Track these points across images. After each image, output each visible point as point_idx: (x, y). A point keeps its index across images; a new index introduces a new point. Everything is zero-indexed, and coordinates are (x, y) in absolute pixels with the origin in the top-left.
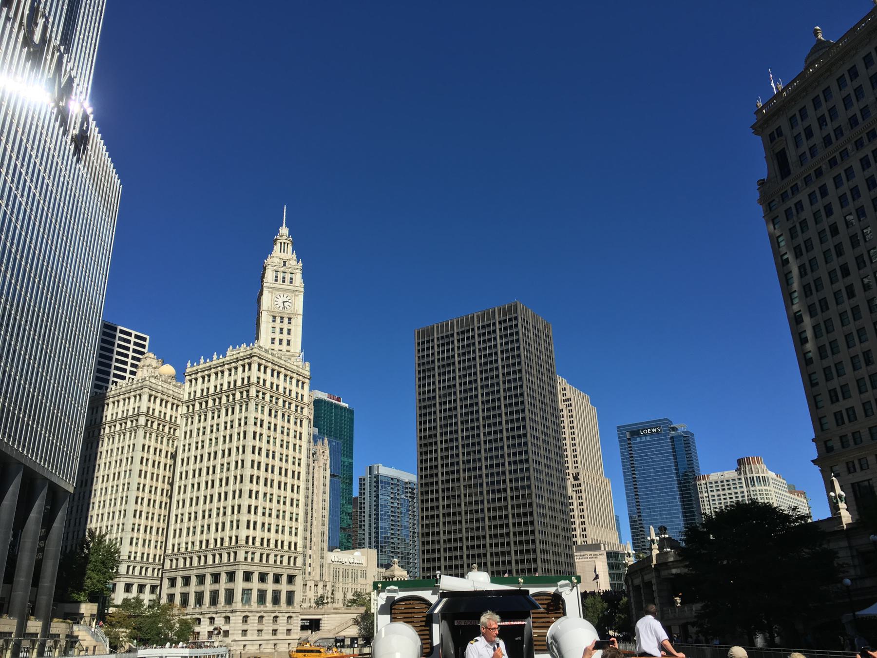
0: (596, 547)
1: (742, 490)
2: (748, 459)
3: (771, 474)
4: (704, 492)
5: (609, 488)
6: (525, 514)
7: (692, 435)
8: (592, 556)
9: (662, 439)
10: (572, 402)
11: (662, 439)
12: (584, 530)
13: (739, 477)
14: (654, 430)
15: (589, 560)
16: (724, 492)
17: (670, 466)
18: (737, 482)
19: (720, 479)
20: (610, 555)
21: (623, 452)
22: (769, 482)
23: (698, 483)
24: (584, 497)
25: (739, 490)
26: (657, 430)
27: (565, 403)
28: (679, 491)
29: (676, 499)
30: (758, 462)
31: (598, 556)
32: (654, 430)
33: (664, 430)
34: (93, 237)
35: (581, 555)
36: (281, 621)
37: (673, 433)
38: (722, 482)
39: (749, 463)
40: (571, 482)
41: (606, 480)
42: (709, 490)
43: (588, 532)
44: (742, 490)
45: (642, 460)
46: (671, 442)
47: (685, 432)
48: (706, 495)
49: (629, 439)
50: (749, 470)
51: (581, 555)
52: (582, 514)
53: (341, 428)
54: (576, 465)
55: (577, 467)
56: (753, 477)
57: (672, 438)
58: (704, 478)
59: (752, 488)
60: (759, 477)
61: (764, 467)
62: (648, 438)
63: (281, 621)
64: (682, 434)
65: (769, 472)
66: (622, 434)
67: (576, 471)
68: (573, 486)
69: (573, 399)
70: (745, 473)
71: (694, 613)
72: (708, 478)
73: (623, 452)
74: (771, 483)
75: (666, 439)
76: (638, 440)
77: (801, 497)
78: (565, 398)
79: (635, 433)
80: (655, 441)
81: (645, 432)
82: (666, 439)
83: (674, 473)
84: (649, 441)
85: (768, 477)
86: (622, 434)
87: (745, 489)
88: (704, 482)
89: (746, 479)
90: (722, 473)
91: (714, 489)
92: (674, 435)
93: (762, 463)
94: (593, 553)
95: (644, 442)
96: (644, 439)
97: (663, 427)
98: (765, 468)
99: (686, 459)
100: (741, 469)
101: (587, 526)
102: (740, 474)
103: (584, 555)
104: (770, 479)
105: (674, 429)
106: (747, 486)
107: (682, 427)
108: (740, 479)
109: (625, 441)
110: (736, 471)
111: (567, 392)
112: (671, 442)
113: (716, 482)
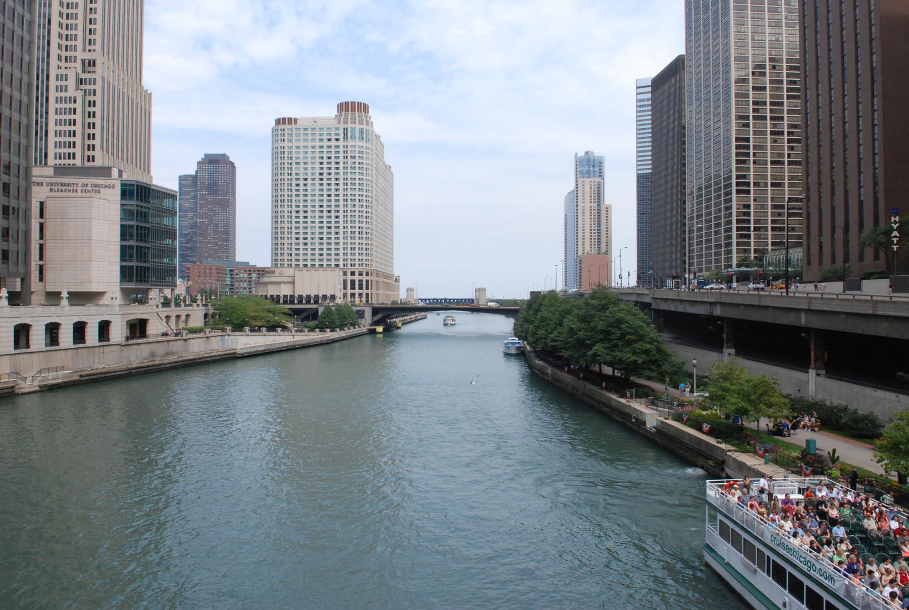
0: (105, 172)
1: (337, 143)
8: (89, 188)
13: (337, 126)
15: (79, 193)
31: (102, 190)
40: (77, 74)
50: (351, 119)
51: (62, 184)
68: (81, 81)
89: (345, 130)
103: (69, 185)
108: (337, 129)
113: (306, 129)
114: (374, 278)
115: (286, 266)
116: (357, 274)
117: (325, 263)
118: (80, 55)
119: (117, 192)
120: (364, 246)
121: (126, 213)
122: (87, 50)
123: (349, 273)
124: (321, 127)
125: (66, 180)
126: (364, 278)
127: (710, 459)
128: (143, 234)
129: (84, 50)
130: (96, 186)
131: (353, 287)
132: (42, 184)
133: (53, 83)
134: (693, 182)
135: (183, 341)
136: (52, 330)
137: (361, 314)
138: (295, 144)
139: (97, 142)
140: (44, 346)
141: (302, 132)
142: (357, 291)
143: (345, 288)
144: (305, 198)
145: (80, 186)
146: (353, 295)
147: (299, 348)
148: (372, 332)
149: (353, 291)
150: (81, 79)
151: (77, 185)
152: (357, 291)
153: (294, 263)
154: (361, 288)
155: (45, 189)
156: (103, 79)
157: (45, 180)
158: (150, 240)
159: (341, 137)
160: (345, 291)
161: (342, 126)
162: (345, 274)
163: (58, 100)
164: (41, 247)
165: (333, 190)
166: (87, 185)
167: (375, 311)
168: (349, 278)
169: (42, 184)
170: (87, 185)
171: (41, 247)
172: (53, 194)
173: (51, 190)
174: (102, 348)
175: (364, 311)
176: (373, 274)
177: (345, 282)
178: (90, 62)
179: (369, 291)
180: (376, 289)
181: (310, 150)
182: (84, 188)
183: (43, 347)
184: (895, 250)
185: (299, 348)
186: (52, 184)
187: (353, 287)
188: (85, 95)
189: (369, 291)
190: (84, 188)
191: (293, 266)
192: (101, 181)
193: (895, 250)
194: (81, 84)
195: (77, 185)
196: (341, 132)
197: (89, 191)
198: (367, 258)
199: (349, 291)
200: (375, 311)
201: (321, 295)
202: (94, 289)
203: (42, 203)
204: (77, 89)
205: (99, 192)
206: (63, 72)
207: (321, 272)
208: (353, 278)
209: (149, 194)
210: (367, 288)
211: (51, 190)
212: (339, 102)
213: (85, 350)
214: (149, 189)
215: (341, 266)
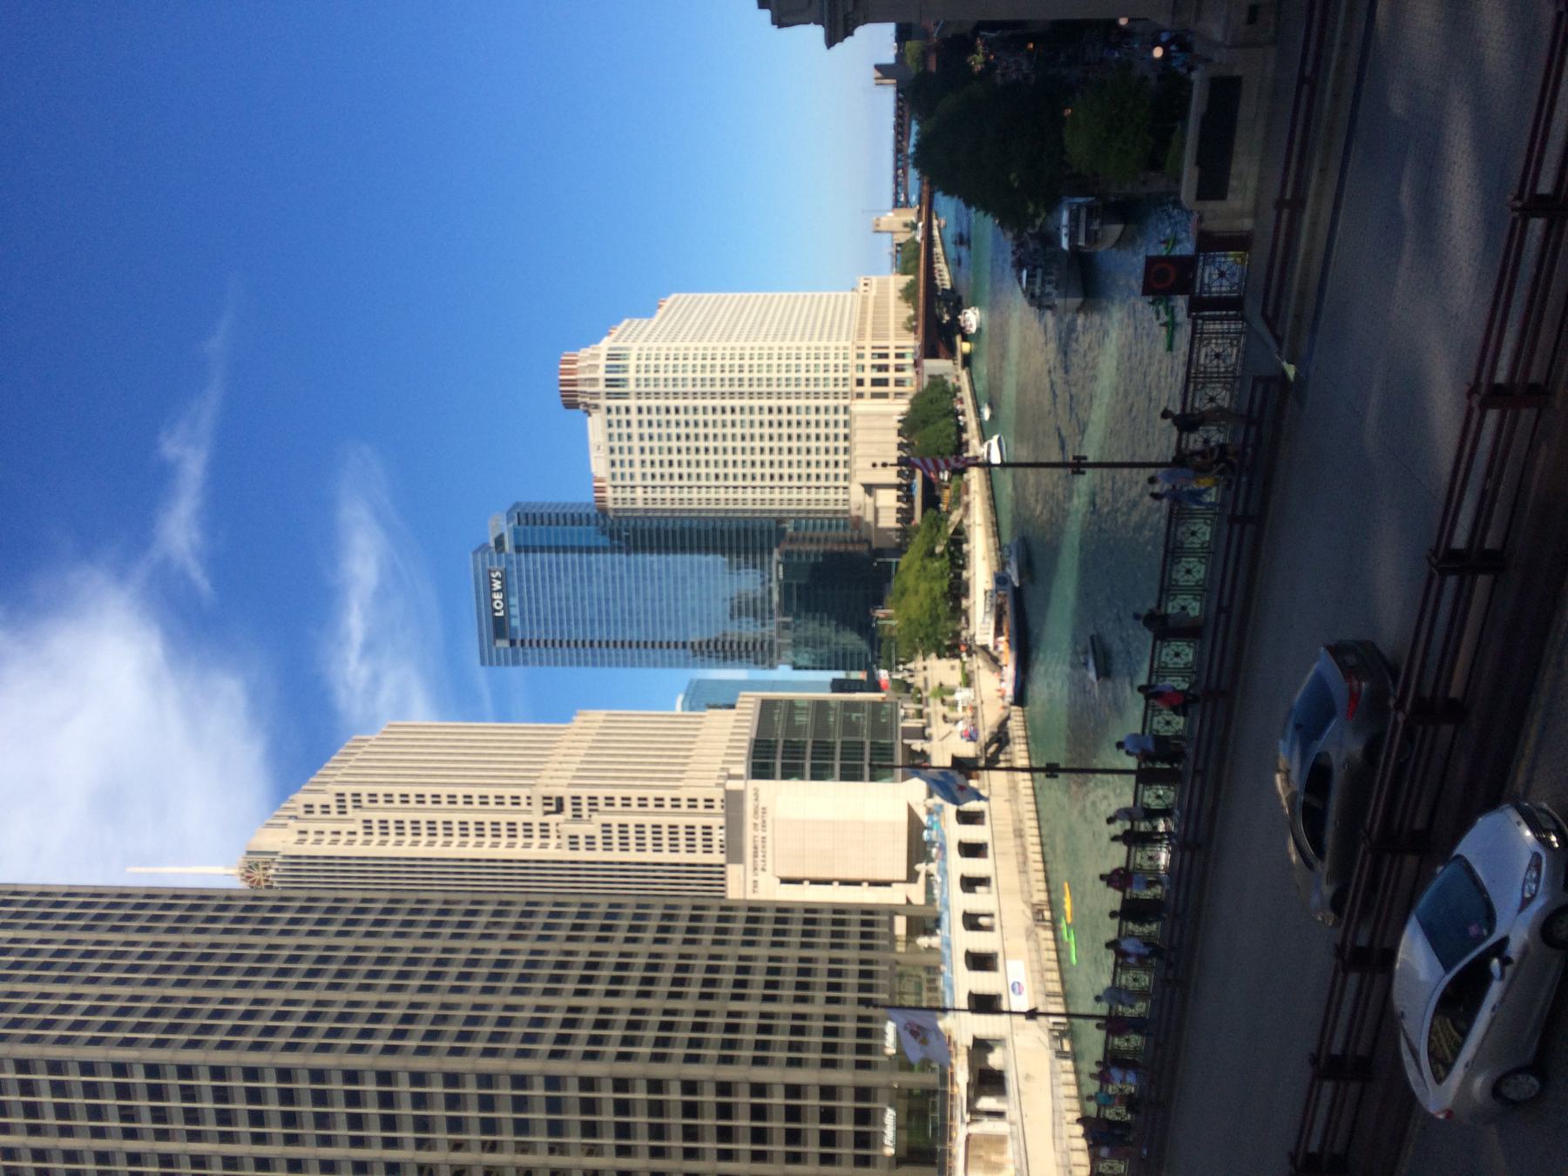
0: (734, 802)
1: (634, 410)
3: (606, 344)
4: (633, 496)
5: (598, 716)
7: (517, 505)
8: (759, 821)
9: (519, 570)
10: (348, 790)
11: (519, 570)
12: (692, 802)
13: (604, 410)
14: (497, 585)
15: (768, 834)
16: (637, 464)
19: (604, 452)
20: (761, 770)
21: (533, 660)
22: (621, 349)
23: (610, 505)
24: (609, 792)
25: (634, 416)
26: (497, 578)
27: (349, 808)
28: (628, 553)
30: (573, 362)
31: (761, 806)
32: (497, 585)
35: (755, 856)
36: (749, 718)
38: (612, 451)
39: (573, 383)
40: (567, 822)
41: (578, 721)
42: (628, 482)
43: (701, 795)
44: (634, 410)
48: (639, 491)
49: (513, 643)
50: (590, 386)
51: (755, 856)
53: (826, 395)
55: (529, 798)
56: (607, 380)
57: (518, 549)
59: (632, 388)
61: (584, 353)
62: (514, 601)
63: (749, 718)
64: (511, 525)
65: (601, 345)
68: (577, 816)
69: (340, 789)
70: (596, 395)
71: (1122, 500)
72: (601, 480)
73: (533, 660)
74: (624, 345)
75: (519, 563)
76: (515, 622)
79: (500, 627)
80: (520, 591)
82: (519, 563)
83: (580, 557)
84: (521, 600)
85: (610, 349)
87: (633, 403)
89: (609, 396)
90: (592, 448)
91: (627, 470)
92: (513, 544)
94: (749, 819)
95: (522, 613)
96: (515, 611)
97: (491, 564)
98: (589, 351)
99: (569, 527)
100: (586, 405)
101: (684, 794)
102: (596, 407)
103: (755, 848)
105: (499, 542)
106: (625, 395)
107: (499, 525)
108: (609, 410)
109: (516, 654)
110: (590, 415)
111: (317, 800)
113: (613, 464)
114: (868, 343)
115: (846, 497)
116: (860, 375)
117: (841, 431)
118: (536, 817)
119: (763, 785)
122: (529, 808)
123: (860, 389)
125: (749, 851)
128: (823, 750)
129: (529, 812)
130: (756, 812)
131: (884, 382)
133: (582, 855)
134: (1342, 927)
137: (937, 382)
139: (667, 795)
141: (618, 470)
143: (885, 395)
144: (730, 464)
146: (899, 382)
147: (991, 480)
149: (892, 382)
153: (841, 483)
154: (884, 368)
155: (761, 877)
156: (570, 785)
157: (750, 877)
158: (831, 740)
159: (622, 403)
162: (860, 396)
163: (607, 845)
165: (763, 470)
166: (755, 825)
168: (867, 388)
169: (755, 882)
170: (755, 825)
172: (769, 867)
173: (763, 870)
175: (930, 376)
177: (874, 396)
178: (546, 804)
179: (892, 352)
180: (886, 337)
181: (648, 457)
182: (760, 827)
185: (991, 480)
186: (755, 869)
187: (884, 382)
189: (892, 352)
191: (846, 484)
192: (749, 806)
196: (613, 403)
198: (832, 356)
199: (891, 388)
203: (785, 881)
204: (589, 821)
206: (565, 841)
208: (868, 382)
210: (886, 356)
211: (763, 870)
212: (563, 408)
214: (756, 741)
215: (846, 402)
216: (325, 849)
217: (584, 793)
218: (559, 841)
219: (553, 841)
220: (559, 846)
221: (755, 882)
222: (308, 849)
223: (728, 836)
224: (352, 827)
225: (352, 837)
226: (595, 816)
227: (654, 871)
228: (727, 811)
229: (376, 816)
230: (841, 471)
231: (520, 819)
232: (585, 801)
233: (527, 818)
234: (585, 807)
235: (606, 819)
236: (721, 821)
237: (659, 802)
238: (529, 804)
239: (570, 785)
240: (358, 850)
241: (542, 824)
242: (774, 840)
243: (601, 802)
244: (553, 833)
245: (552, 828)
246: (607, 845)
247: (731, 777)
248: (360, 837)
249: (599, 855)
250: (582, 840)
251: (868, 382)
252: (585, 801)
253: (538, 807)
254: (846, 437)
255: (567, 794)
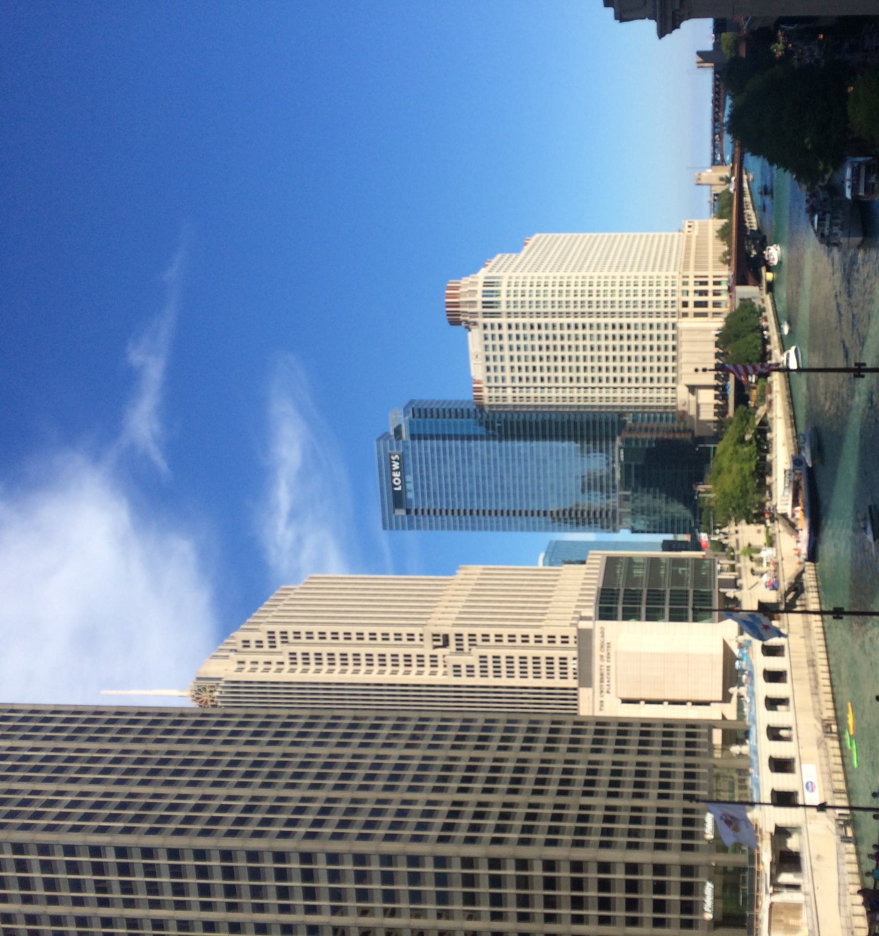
0: (584, 638)
1: (505, 327)
2: (449, 305)
3: (483, 274)
4: (504, 395)
5: (476, 570)
6: (469, 880)
8: (605, 654)
9: (414, 454)
10: (277, 629)
11: (414, 454)
13: (481, 327)
14: (396, 466)
15: (612, 664)
17: (551, 449)
18: (489, 332)
20: (606, 613)
21: (425, 525)
24: (485, 631)
26: (396, 460)
29: (557, 448)
30: (457, 288)
31: (607, 640)
32: (396, 466)
33: (398, 448)
34: (498, 604)
37: (405, 434)
38: (487, 359)
39: (457, 305)
40: (452, 654)
41: (461, 574)
42: (500, 384)
43: (558, 632)
45: (453, 494)
46: (419, 439)
47: (405, 413)
48: (509, 390)
49: (408, 512)
50: (470, 307)
51: (602, 681)
52: (519, 639)
54: (417, 637)
55: (421, 635)
57: (413, 437)
58: (479, 390)
59: (503, 308)
60: (484, 291)
62: (409, 478)
64: (407, 418)
66: (397, 522)
67: (428, 639)
68: (460, 650)
69: (271, 628)
70: (474, 314)
72: (479, 382)
73: (425, 525)
75: (413, 448)
76: (411, 495)
77: (528, 240)
78: (266, 644)
79: (398, 499)
81: (397, 481)
82: (413, 448)
84: (415, 477)
85: (486, 278)
86: (397, 522)
87: (504, 321)
88: (486, 390)
89: (485, 315)
93: (459, 283)
94: (597, 652)
95: (416, 487)
96: (410, 486)
97: (391, 449)
100: (467, 322)
101: (545, 632)
103: (602, 675)
104: (491, 274)
105: (398, 431)
106: (498, 315)
108: (485, 327)
110: (470, 330)
111: (253, 637)
112: (419, 439)
113: (488, 369)
114: (691, 273)
116: (685, 299)
118: (427, 650)
119: (608, 624)
120: (647, 288)
121: (630, 614)
122: (421, 643)
123: (685, 310)
124: (483, 348)
126: (691, 287)
127: (838, 725)
129: (421, 646)
130: (602, 647)
132: (602, 702)
133: (464, 680)
135: (784, 562)
136: (772, 703)
137: (747, 304)
138: (508, 383)
139: (532, 632)
140: (789, 713)
142: (710, 298)
143: (705, 315)
145: (602, 663)
148: (770, 287)
150: (458, 649)
151: (601, 666)
152: (710, 298)
153: (670, 384)
156: (454, 625)
157: (598, 698)
160: (710, 315)
161: (481, 320)
162: (685, 315)
163: (484, 673)
164: (673, 702)
167: (741, 279)
168: (691, 309)
171: (673, 702)
172: (612, 690)
173: (608, 692)
174: (791, 654)
176: (686, 273)
177: (697, 315)
179: (711, 280)
180: (706, 268)
182: (605, 658)
183: (791, 714)
184: (752, 256)
186: (602, 692)
187: (704, 304)
188: (475, 645)
189: (711, 280)
190: (605, 658)
191: (674, 385)
192: (597, 641)
193: (752, 256)
194: (462, 650)
195: (601, 666)
197: (608, 654)
199: (710, 309)
200: (741, 279)
201: (716, 350)
202: (720, 651)
203: (625, 701)
204: (469, 654)
205: (608, 644)
206: (450, 669)
207: (684, 348)
208: (691, 304)
209: (608, 590)
210: (706, 283)
211: (608, 692)
212: (448, 325)
213: (793, 671)
215: (674, 320)
216: (259, 676)
217: (466, 631)
218: (445, 669)
219: (440, 670)
220: (445, 674)
221: (602, 702)
222: (245, 675)
223: (580, 665)
224: (280, 658)
225: (280, 666)
226: (474, 649)
227: (521, 693)
228: (579, 645)
229: (299, 650)
230: (670, 375)
231: (414, 652)
232: (466, 638)
233: (420, 651)
234: (466, 643)
235: (483, 652)
236: (575, 653)
237: (373, 636)
238: (421, 640)
239: (454, 625)
240: (285, 676)
241: (431, 656)
242: (616, 668)
243: (479, 638)
244: (440, 663)
245: (440, 659)
246: (484, 673)
247: (582, 618)
248: (287, 666)
249: (477, 680)
250: (464, 669)
251: (691, 304)
252: (466, 638)
253: (428, 642)
254: (674, 348)
255: (452, 632)
